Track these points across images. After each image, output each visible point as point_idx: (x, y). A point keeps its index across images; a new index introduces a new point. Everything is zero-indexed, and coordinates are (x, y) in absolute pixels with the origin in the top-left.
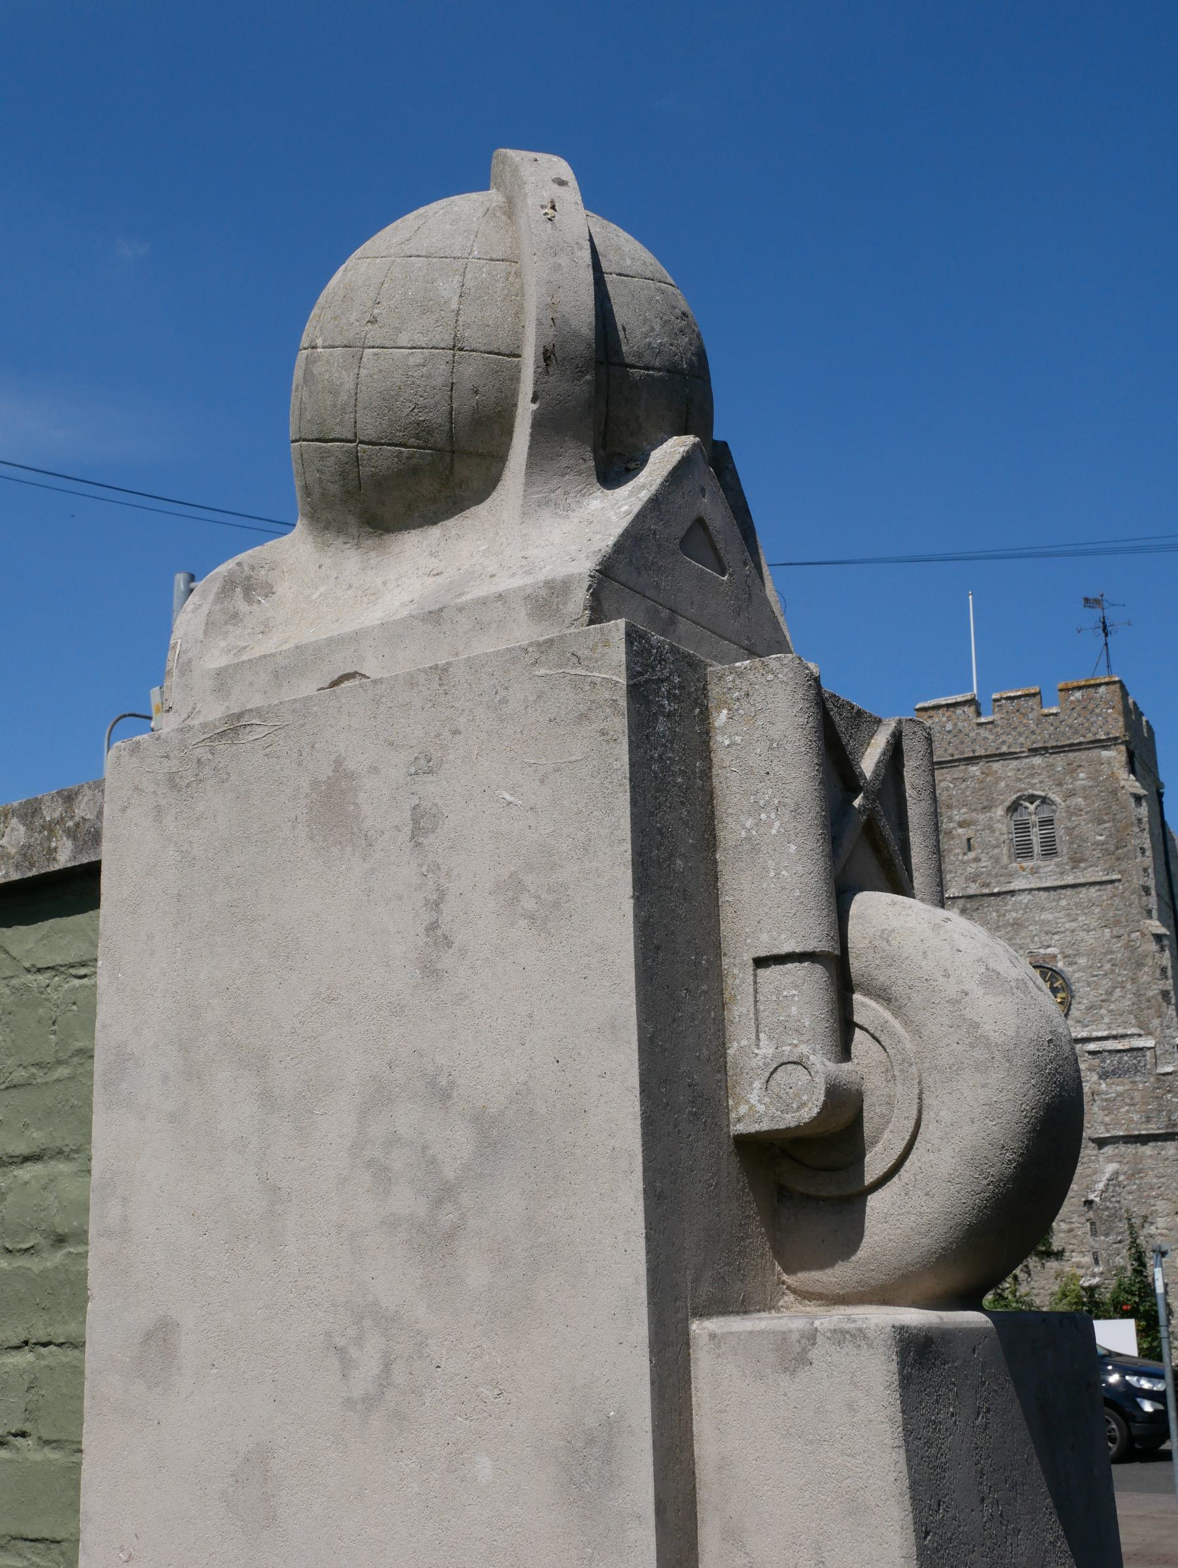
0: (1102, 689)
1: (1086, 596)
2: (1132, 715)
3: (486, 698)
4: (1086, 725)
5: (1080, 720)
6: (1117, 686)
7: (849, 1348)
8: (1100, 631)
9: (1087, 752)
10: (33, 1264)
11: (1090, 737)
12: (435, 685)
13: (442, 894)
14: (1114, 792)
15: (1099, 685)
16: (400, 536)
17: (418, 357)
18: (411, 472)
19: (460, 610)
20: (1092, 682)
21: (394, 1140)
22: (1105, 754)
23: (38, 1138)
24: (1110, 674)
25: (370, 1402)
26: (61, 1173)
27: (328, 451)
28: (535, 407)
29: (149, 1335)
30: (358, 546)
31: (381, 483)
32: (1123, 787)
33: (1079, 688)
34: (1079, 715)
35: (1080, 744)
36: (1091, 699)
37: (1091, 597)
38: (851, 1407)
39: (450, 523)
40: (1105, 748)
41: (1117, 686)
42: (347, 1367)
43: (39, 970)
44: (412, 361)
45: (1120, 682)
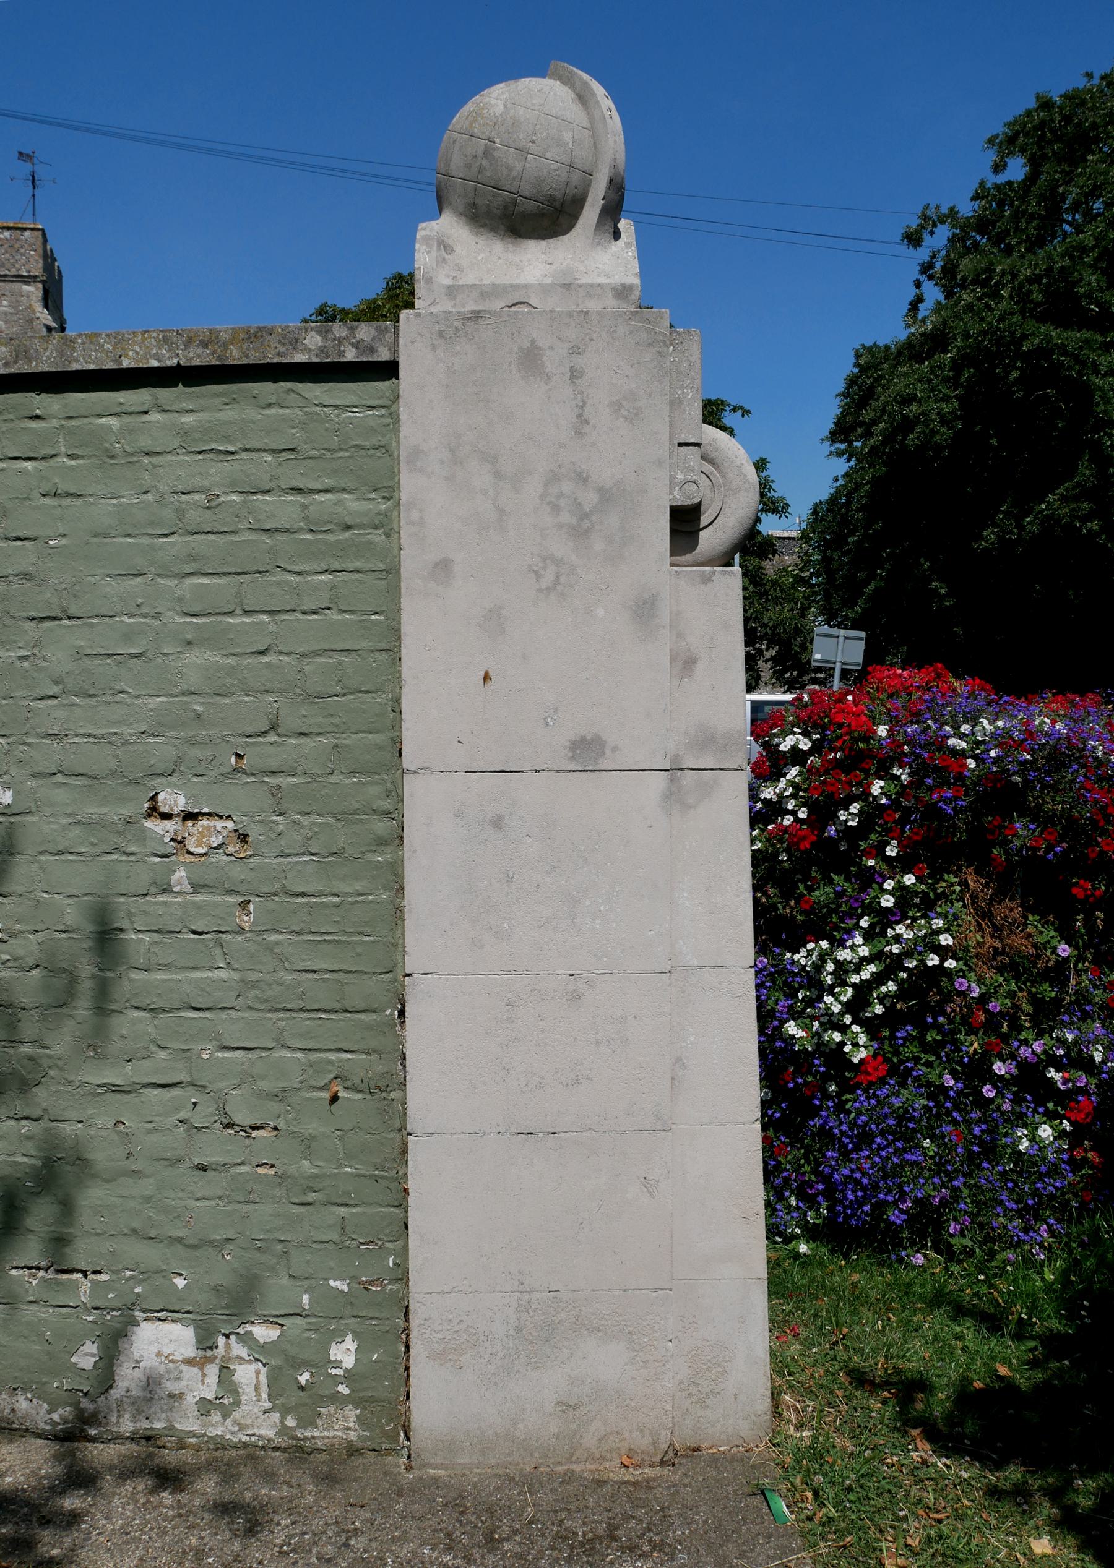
0: (27, 233)
1: (21, 150)
2: (49, 259)
3: (606, 329)
4: (12, 261)
5: (7, 256)
6: (40, 232)
7: (727, 576)
8: (30, 183)
9: (10, 284)
10: (330, 538)
11: (14, 272)
12: (582, 318)
13: (585, 404)
14: (30, 321)
15: (25, 229)
16: (526, 241)
17: (555, 166)
18: (542, 215)
19: (580, 286)
20: (20, 226)
21: (561, 495)
22: (25, 288)
23: (328, 482)
24: (34, 222)
25: (549, 590)
26: (346, 499)
27: (500, 194)
28: (602, 202)
29: (437, 565)
30: (502, 240)
31: (525, 216)
32: (38, 318)
33: (9, 228)
34: (6, 252)
35: (5, 276)
36: (18, 240)
37: (25, 151)
38: (727, 595)
39: (551, 241)
40: (27, 283)
41: (40, 232)
42: (538, 577)
43: (324, 406)
44: (552, 167)
45: (43, 230)
